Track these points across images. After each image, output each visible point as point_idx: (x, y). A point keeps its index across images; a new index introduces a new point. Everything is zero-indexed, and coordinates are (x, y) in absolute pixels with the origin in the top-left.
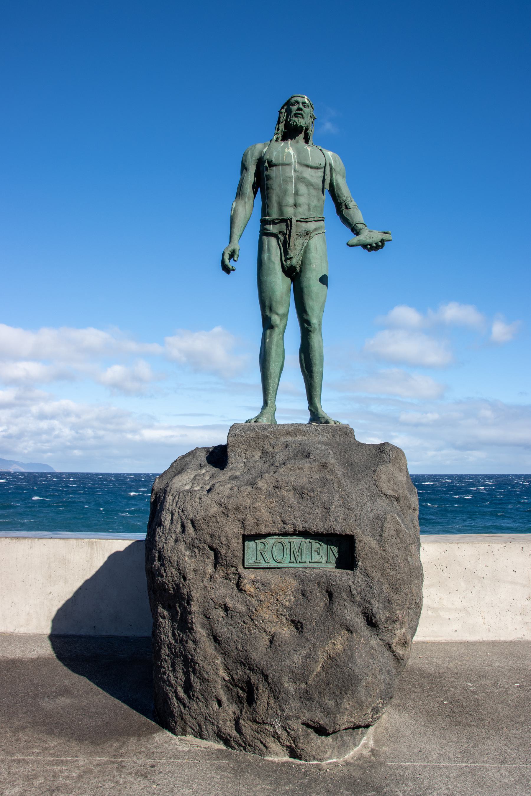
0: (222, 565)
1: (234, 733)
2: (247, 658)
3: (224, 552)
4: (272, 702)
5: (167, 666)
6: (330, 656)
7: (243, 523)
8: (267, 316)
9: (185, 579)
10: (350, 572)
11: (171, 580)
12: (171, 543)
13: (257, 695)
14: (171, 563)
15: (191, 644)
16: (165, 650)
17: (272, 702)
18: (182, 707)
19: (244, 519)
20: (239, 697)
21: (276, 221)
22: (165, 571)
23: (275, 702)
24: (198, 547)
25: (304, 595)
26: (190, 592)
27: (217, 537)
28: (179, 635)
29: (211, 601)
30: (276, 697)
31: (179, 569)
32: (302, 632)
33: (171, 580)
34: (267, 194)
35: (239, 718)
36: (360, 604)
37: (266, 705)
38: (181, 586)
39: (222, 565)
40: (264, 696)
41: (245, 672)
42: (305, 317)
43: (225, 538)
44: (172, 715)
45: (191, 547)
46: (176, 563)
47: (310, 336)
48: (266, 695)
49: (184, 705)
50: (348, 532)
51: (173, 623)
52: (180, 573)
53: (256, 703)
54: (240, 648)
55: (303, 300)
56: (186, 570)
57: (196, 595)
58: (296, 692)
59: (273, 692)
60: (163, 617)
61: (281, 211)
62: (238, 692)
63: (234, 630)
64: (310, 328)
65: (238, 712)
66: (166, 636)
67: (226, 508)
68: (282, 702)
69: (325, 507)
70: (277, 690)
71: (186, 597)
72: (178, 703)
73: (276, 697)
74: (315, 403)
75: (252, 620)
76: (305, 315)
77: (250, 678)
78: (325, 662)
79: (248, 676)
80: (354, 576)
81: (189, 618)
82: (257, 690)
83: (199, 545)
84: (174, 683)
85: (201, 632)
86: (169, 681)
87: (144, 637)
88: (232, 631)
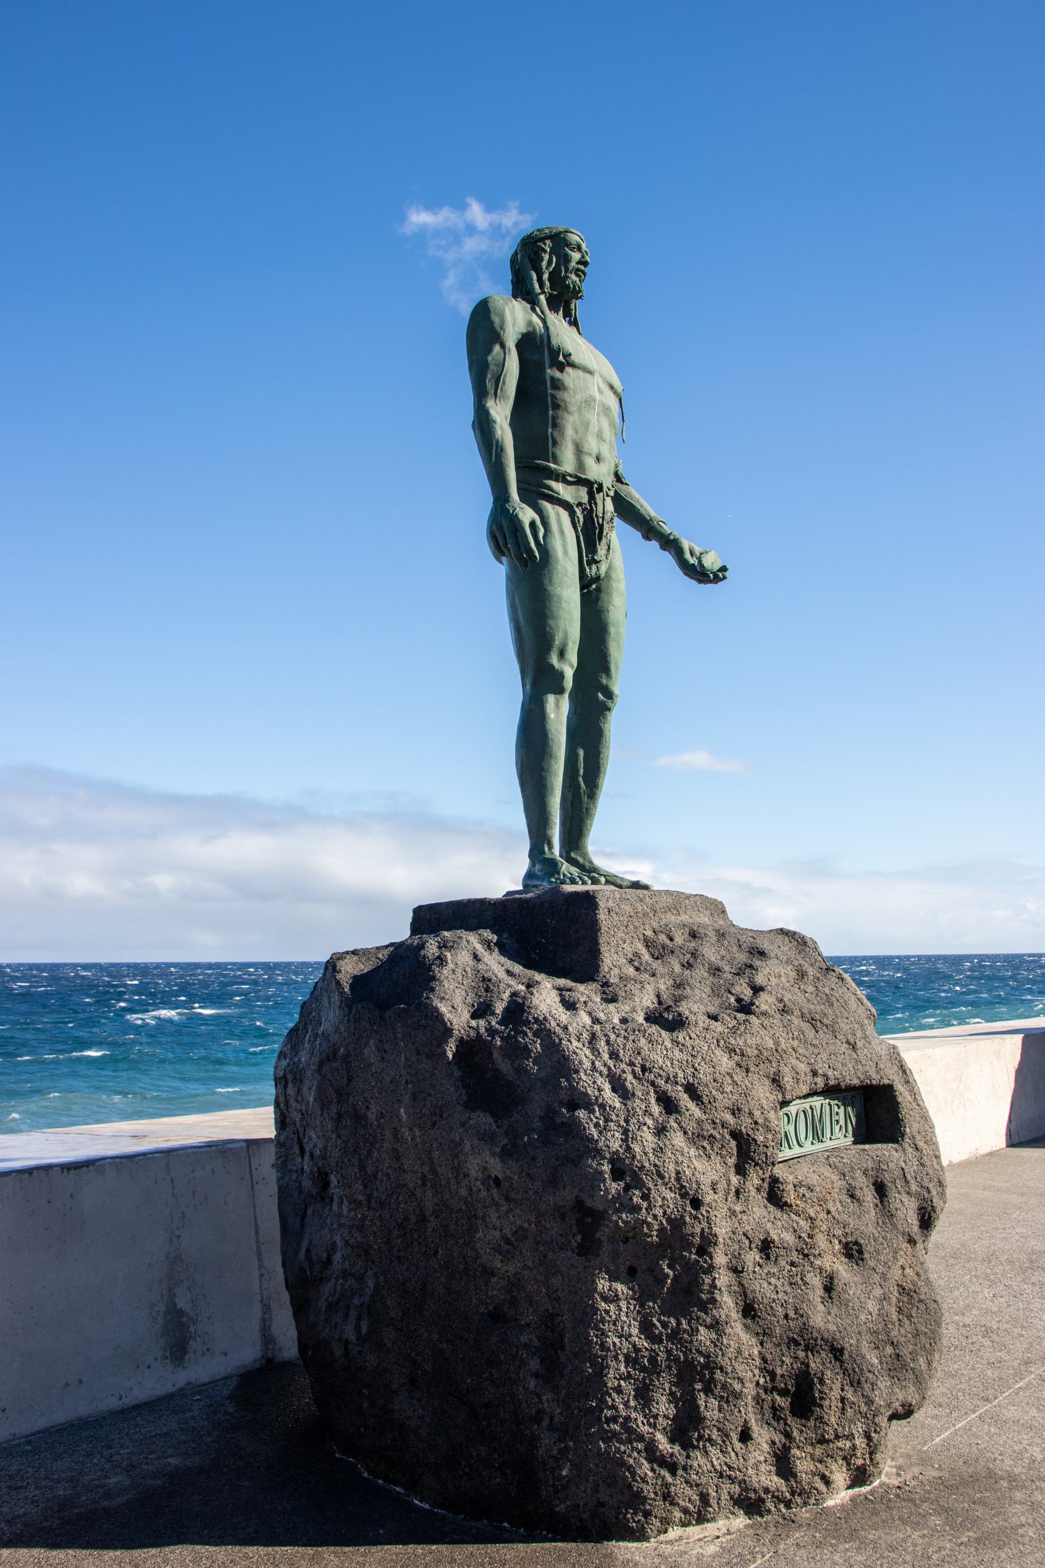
0: (757, 1164)
1: (775, 1482)
2: (805, 1328)
3: (761, 1138)
4: (849, 1394)
5: (622, 1402)
6: (904, 1289)
7: (774, 1080)
8: (553, 666)
9: (696, 1203)
10: (895, 1146)
11: (659, 1212)
12: (648, 1137)
13: (821, 1392)
14: (662, 1177)
15: (704, 1336)
16: (616, 1370)
17: (849, 1394)
18: (667, 1475)
19: (778, 1073)
20: (775, 1409)
21: (569, 478)
22: (645, 1197)
23: (855, 1391)
24: (711, 1136)
25: (852, 1196)
26: (710, 1228)
27: (747, 1111)
28: (665, 1325)
29: (744, 1238)
30: (855, 1384)
31: (682, 1187)
32: (862, 1260)
33: (659, 1212)
34: (554, 418)
35: (786, 1449)
36: (917, 1195)
37: (840, 1405)
38: (687, 1219)
39: (757, 1164)
40: (833, 1388)
41: (797, 1358)
42: (604, 681)
43: (759, 1112)
44: (636, 1500)
45: (696, 1138)
46: (673, 1175)
47: (605, 718)
48: (838, 1385)
49: (673, 1469)
50: (886, 1082)
51: (642, 1306)
52: (684, 1196)
53: (821, 1406)
54: (792, 1314)
55: (606, 648)
56: (702, 1187)
57: (722, 1229)
58: (881, 1363)
59: (849, 1375)
60: (615, 1299)
61: (581, 465)
62: (773, 1401)
63: (779, 1284)
64: (609, 704)
65: (779, 1438)
66: (620, 1337)
67: (743, 1055)
68: (867, 1386)
69: (848, 1042)
70: (857, 1370)
71: (697, 1240)
72: (653, 1470)
73: (855, 1384)
74: (585, 847)
75: (806, 1256)
76: (604, 676)
77: (808, 1365)
78: (899, 1301)
79: (802, 1363)
80: (904, 1150)
81: (707, 1281)
82: (821, 1381)
83: (715, 1133)
84: (645, 1429)
85: (728, 1305)
86: (630, 1431)
87: (39, 1432)
88: (776, 1286)
